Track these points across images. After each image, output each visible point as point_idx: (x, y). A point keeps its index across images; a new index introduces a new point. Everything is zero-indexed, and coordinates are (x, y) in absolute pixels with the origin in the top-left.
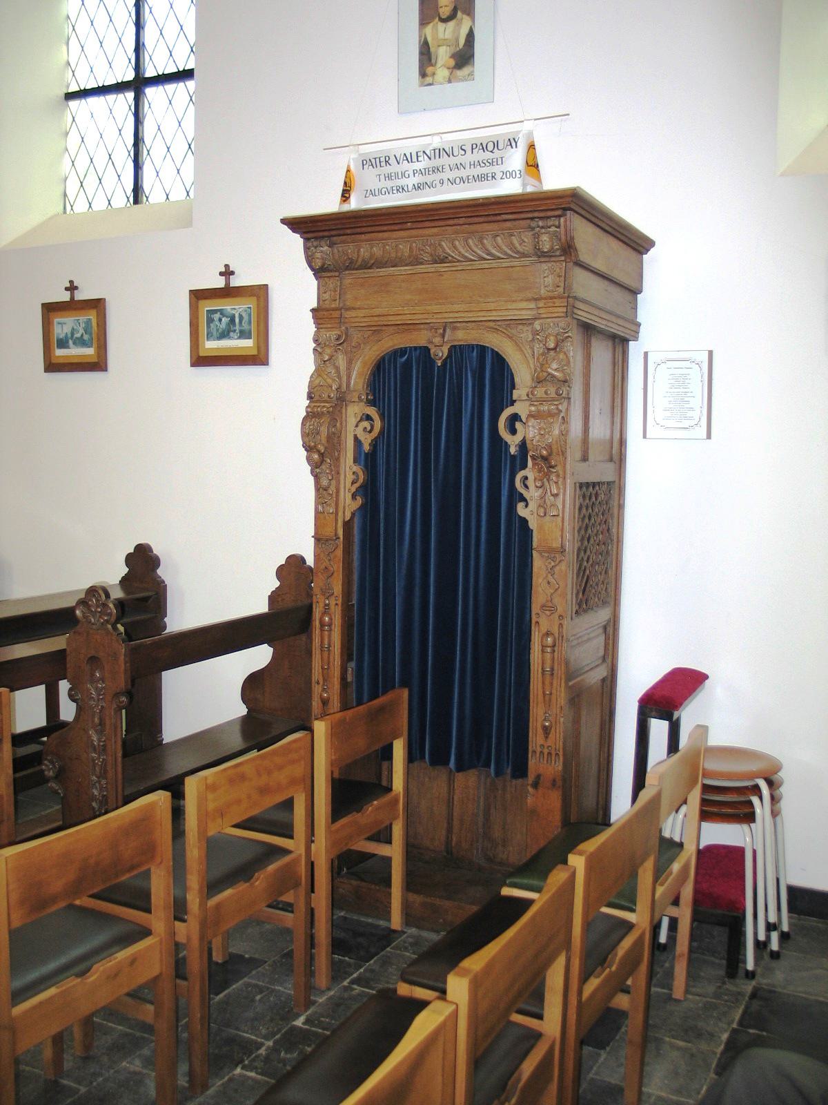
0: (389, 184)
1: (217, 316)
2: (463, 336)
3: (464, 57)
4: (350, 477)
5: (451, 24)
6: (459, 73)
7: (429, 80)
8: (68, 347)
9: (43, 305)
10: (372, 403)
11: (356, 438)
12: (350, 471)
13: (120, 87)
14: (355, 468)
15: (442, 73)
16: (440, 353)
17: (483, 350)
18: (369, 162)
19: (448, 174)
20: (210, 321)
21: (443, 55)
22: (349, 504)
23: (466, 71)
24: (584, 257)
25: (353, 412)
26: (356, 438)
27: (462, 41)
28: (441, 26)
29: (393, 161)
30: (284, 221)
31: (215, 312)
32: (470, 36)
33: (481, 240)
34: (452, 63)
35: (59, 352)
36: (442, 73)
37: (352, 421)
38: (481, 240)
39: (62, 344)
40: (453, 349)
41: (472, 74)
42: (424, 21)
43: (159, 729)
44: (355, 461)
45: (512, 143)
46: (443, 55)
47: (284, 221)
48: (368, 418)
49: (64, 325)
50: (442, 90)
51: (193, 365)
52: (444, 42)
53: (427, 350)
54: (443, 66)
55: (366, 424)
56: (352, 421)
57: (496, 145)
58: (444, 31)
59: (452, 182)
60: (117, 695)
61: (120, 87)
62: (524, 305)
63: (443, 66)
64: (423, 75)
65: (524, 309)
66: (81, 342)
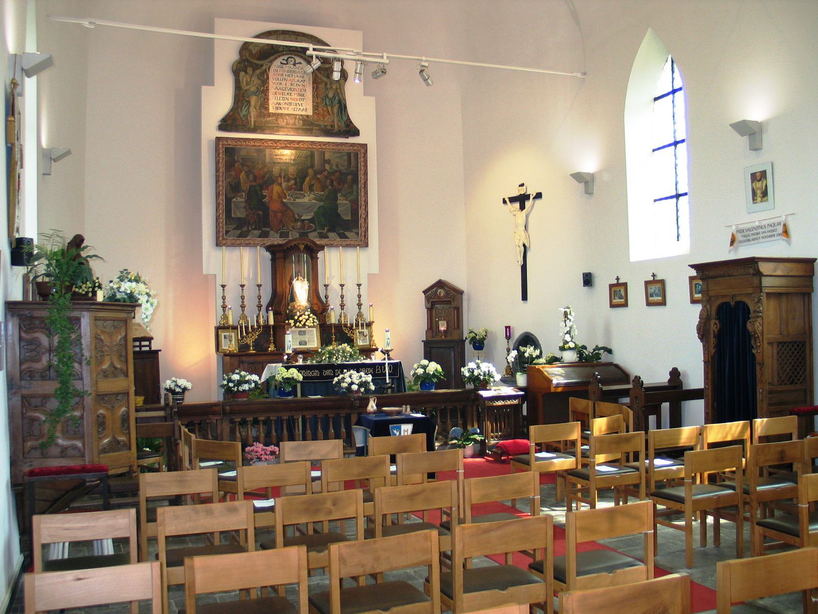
0: (745, 239)
1: (698, 285)
2: (738, 299)
3: (765, 194)
4: (712, 342)
5: (760, 182)
6: (764, 199)
7: (755, 201)
8: (653, 297)
9: (645, 282)
10: (716, 319)
11: (713, 330)
12: (712, 340)
13: (671, 197)
14: (714, 339)
15: (759, 199)
16: (733, 303)
17: (744, 303)
18: (738, 231)
19: (762, 235)
20: (696, 287)
21: (759, 193)
22: (713, 351)
23: (766, 198)
24: (765, 274)
25: (713, 321)
26: (713, 330)
27: (764, 188)
28: (757, 183)
29: (745, 231)
30: (689, 266)
31: (697, 284)
32: (766, 186)
33: (737, 270)
34: (761, 195)
35: (651, 299)
36: (759, 199)
37: (712, 325)
38: (737, 270)
39: (652, 296)
40: (736, 302)
41: (767, 199)
42: (752, 182)
43: (204, 85)
44: (714, 337)
45: (779, 224)
46: (759, 193)
47: (689, 266)
48: (716, 324)
49: (653, 289)
50: (760, 205)
51: (691, 303)
52: (758, 189)
53: (729, 303)
54: (759, 197)
55: (715, 326)
56: (712, 325)
57: (774, 225)
58: (759, 184)
59: (763, 238)
60: (642, 407)
61: (671, 197)
62: (750, 289)
63: (759, 197)
64: (754, 200)
65: (750, 290)
66: (657, 295)
